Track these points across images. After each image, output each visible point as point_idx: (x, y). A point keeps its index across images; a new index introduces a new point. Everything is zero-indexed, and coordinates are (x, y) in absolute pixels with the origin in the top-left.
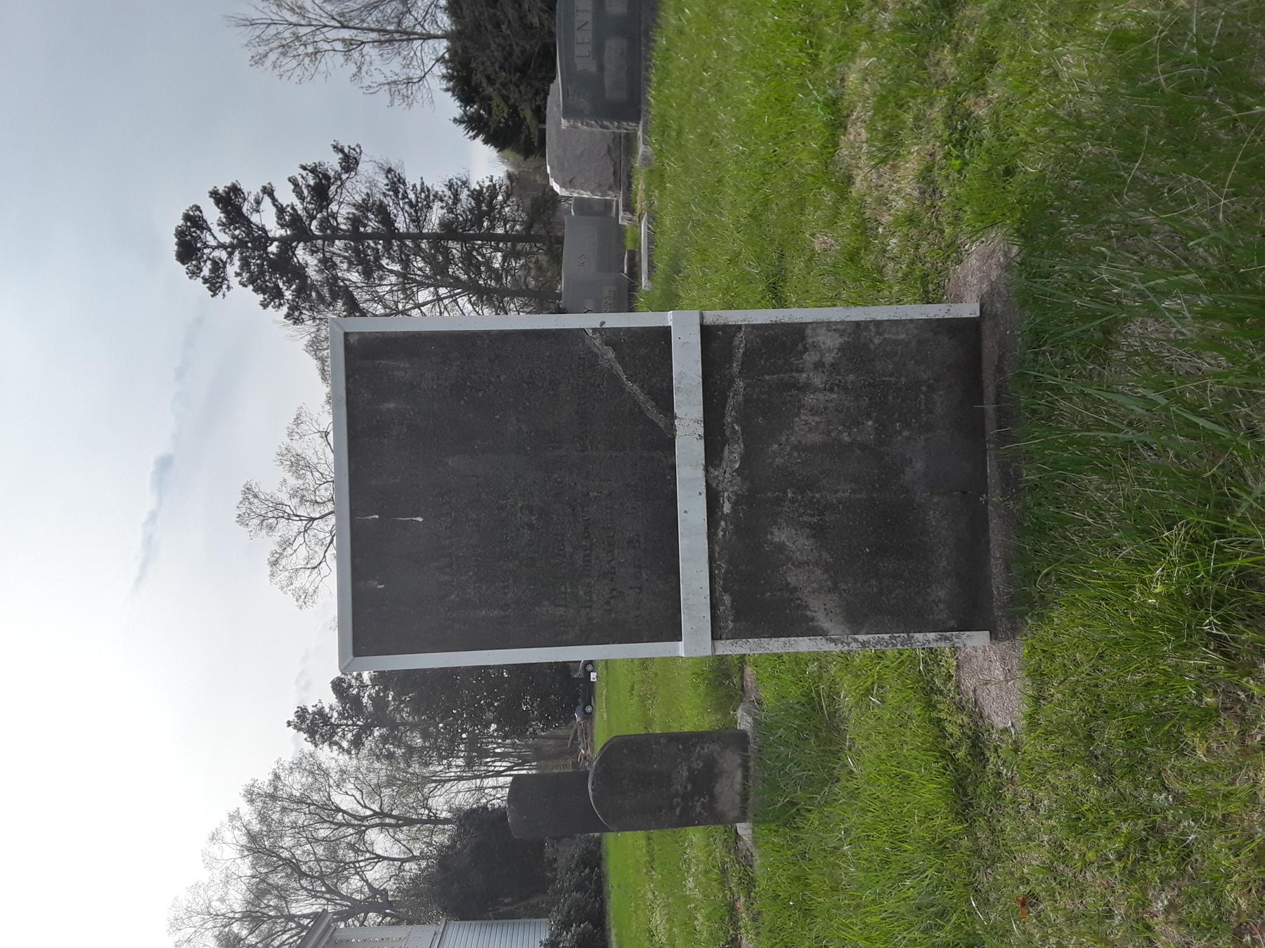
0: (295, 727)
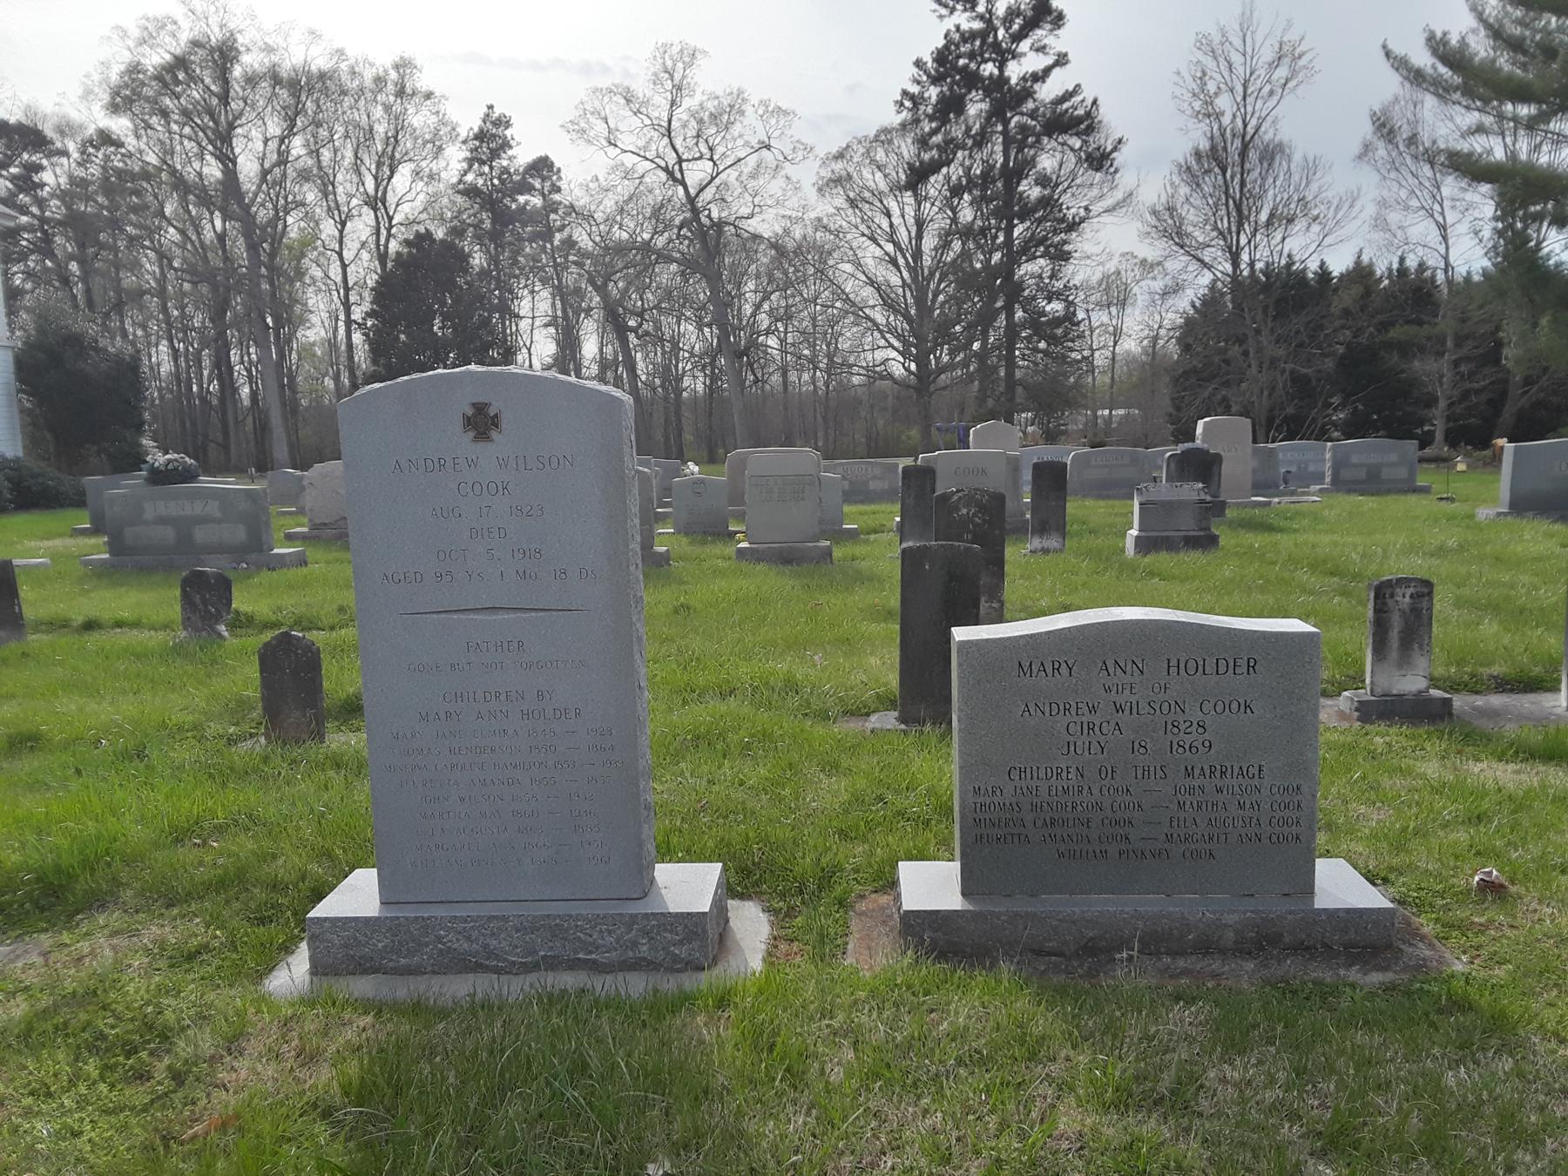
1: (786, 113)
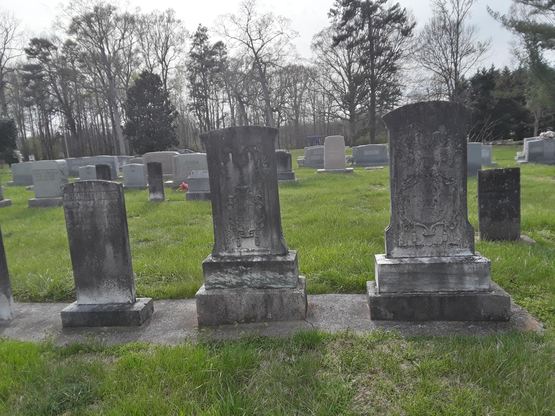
0: (199, 27)
1: (288, 20)
